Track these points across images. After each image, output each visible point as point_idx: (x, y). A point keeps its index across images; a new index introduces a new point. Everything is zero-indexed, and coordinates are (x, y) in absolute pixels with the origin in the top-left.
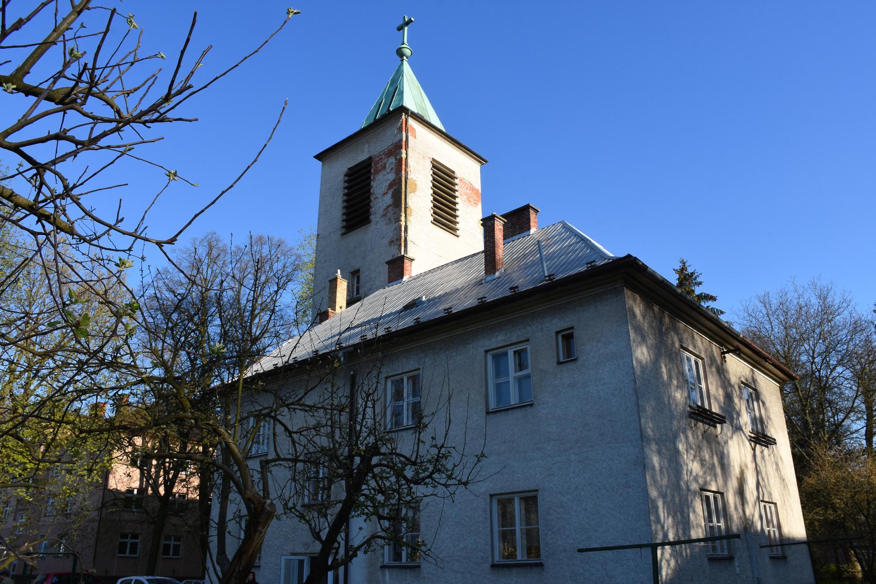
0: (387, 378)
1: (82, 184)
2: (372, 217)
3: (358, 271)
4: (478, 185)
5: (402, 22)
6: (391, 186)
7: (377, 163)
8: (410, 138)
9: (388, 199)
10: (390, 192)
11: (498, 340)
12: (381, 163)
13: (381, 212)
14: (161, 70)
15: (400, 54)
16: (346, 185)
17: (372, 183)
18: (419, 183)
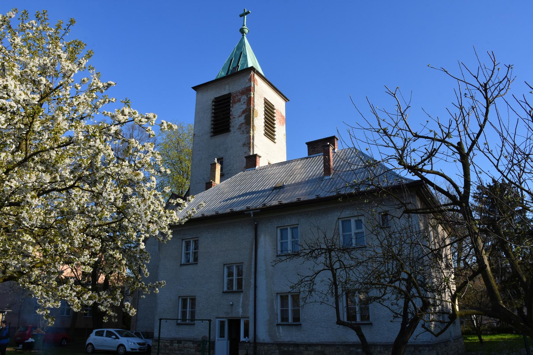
0: (277, 227)
1: (485, 155)
2: (231, 129)
3: (222, 158)
4: (284, 114)
5: (243, 12)
6: (244, 112)
7: (234, 97)
8: (255, 85)
9: (242, 119)
10: (243, 116)
11: (346, 213)
12: (237, 98)
13: (237, 126)
14: (72, 22)
15: (242, 31)
16: (214, 107)
17: (231, 109)
18: (259, 112)
